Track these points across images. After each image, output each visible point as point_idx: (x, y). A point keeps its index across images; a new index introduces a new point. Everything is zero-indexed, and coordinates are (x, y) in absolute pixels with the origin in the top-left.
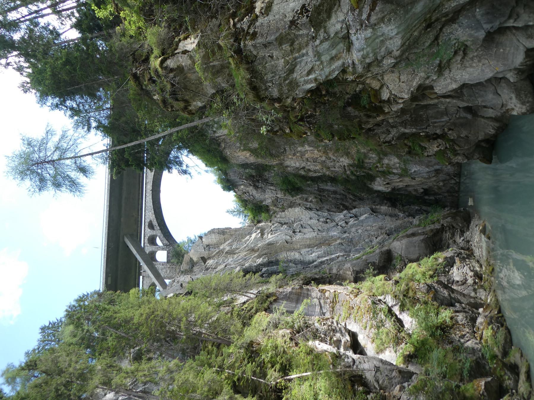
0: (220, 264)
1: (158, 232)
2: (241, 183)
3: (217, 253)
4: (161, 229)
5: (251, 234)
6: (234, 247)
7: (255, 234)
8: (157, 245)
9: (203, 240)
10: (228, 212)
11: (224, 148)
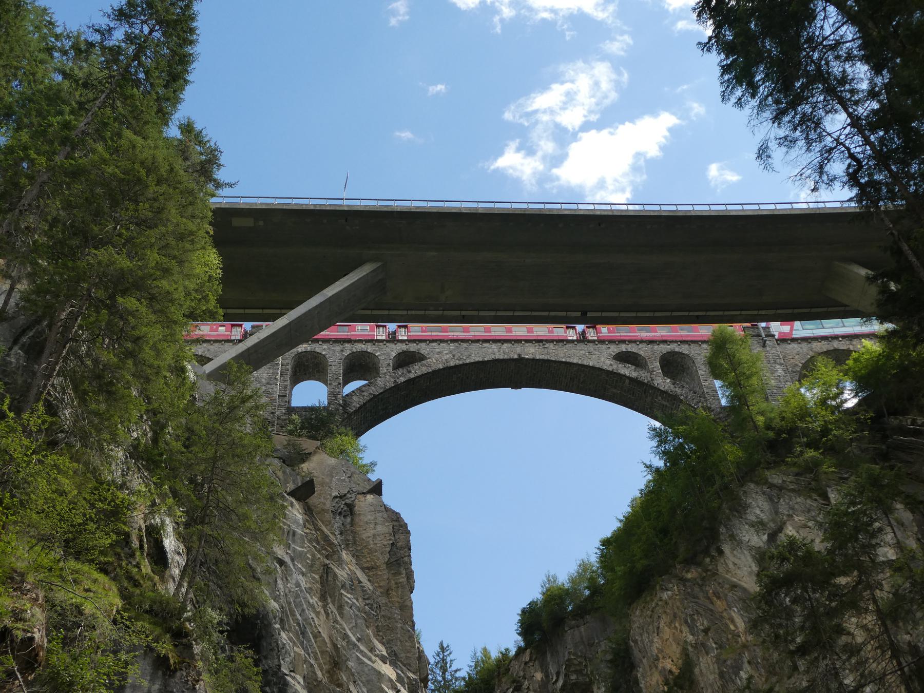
0: (289, 546)
1: (386, 380)
2: (552, 670)
3: (326, 538)
4: (397, 388)
5: (393, 664)
6: (348, 596)
7: (393, 677)
8: (346, 382)
9: (370, 497)
10: (443, 649)
11: (683, 580)
